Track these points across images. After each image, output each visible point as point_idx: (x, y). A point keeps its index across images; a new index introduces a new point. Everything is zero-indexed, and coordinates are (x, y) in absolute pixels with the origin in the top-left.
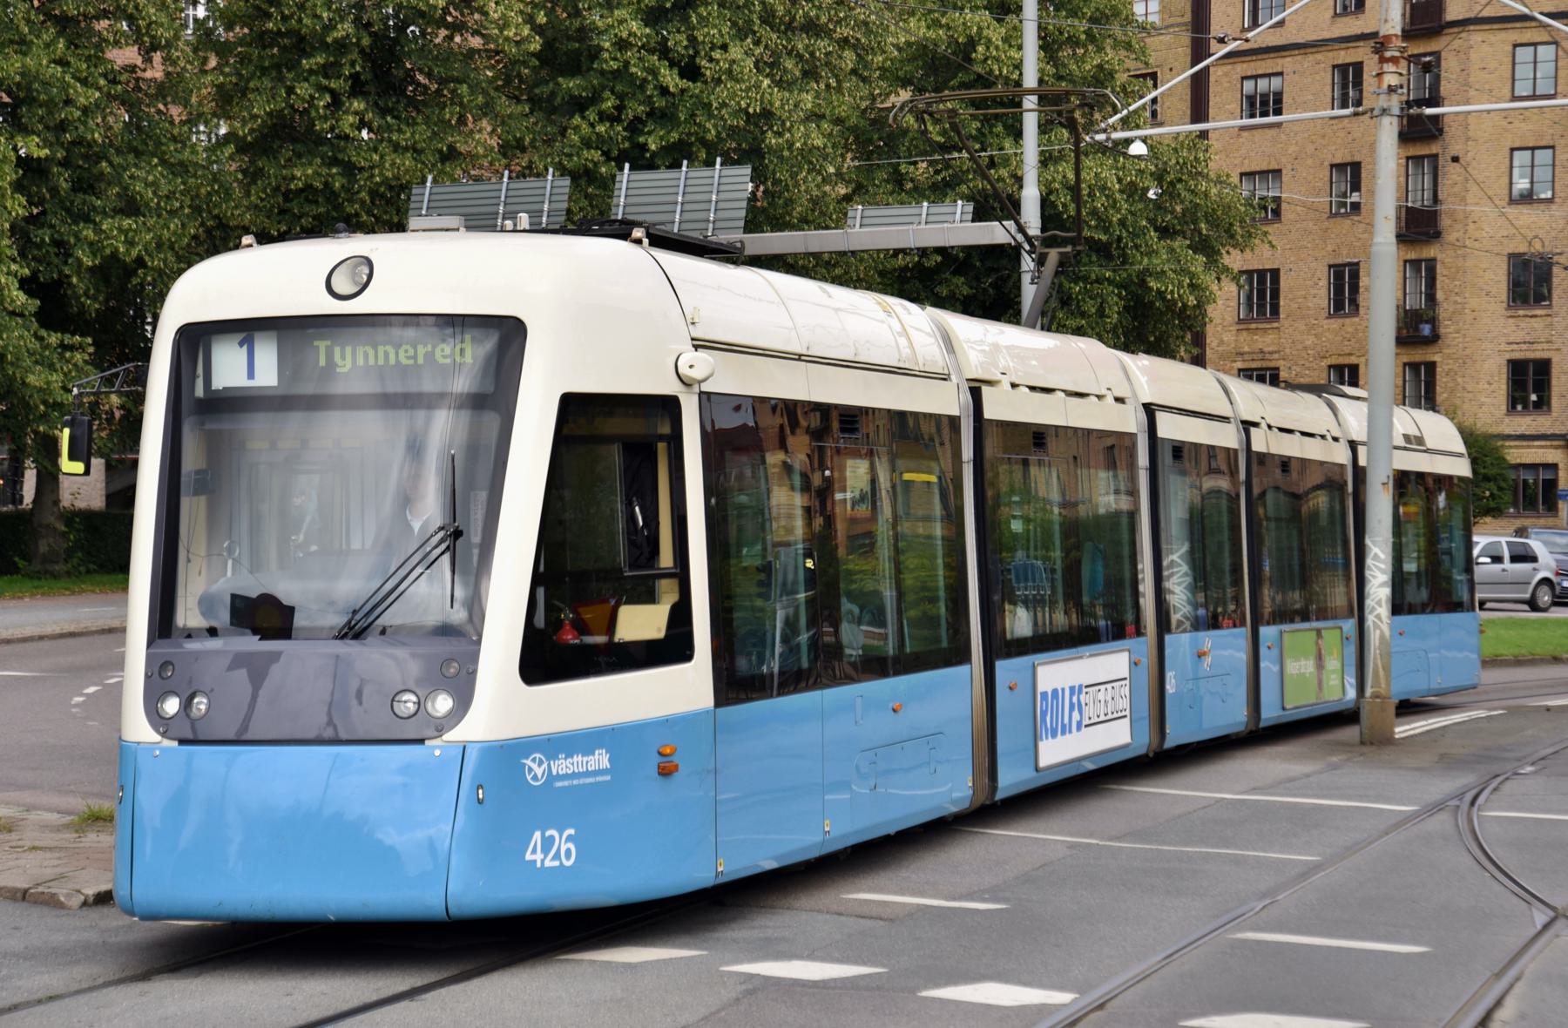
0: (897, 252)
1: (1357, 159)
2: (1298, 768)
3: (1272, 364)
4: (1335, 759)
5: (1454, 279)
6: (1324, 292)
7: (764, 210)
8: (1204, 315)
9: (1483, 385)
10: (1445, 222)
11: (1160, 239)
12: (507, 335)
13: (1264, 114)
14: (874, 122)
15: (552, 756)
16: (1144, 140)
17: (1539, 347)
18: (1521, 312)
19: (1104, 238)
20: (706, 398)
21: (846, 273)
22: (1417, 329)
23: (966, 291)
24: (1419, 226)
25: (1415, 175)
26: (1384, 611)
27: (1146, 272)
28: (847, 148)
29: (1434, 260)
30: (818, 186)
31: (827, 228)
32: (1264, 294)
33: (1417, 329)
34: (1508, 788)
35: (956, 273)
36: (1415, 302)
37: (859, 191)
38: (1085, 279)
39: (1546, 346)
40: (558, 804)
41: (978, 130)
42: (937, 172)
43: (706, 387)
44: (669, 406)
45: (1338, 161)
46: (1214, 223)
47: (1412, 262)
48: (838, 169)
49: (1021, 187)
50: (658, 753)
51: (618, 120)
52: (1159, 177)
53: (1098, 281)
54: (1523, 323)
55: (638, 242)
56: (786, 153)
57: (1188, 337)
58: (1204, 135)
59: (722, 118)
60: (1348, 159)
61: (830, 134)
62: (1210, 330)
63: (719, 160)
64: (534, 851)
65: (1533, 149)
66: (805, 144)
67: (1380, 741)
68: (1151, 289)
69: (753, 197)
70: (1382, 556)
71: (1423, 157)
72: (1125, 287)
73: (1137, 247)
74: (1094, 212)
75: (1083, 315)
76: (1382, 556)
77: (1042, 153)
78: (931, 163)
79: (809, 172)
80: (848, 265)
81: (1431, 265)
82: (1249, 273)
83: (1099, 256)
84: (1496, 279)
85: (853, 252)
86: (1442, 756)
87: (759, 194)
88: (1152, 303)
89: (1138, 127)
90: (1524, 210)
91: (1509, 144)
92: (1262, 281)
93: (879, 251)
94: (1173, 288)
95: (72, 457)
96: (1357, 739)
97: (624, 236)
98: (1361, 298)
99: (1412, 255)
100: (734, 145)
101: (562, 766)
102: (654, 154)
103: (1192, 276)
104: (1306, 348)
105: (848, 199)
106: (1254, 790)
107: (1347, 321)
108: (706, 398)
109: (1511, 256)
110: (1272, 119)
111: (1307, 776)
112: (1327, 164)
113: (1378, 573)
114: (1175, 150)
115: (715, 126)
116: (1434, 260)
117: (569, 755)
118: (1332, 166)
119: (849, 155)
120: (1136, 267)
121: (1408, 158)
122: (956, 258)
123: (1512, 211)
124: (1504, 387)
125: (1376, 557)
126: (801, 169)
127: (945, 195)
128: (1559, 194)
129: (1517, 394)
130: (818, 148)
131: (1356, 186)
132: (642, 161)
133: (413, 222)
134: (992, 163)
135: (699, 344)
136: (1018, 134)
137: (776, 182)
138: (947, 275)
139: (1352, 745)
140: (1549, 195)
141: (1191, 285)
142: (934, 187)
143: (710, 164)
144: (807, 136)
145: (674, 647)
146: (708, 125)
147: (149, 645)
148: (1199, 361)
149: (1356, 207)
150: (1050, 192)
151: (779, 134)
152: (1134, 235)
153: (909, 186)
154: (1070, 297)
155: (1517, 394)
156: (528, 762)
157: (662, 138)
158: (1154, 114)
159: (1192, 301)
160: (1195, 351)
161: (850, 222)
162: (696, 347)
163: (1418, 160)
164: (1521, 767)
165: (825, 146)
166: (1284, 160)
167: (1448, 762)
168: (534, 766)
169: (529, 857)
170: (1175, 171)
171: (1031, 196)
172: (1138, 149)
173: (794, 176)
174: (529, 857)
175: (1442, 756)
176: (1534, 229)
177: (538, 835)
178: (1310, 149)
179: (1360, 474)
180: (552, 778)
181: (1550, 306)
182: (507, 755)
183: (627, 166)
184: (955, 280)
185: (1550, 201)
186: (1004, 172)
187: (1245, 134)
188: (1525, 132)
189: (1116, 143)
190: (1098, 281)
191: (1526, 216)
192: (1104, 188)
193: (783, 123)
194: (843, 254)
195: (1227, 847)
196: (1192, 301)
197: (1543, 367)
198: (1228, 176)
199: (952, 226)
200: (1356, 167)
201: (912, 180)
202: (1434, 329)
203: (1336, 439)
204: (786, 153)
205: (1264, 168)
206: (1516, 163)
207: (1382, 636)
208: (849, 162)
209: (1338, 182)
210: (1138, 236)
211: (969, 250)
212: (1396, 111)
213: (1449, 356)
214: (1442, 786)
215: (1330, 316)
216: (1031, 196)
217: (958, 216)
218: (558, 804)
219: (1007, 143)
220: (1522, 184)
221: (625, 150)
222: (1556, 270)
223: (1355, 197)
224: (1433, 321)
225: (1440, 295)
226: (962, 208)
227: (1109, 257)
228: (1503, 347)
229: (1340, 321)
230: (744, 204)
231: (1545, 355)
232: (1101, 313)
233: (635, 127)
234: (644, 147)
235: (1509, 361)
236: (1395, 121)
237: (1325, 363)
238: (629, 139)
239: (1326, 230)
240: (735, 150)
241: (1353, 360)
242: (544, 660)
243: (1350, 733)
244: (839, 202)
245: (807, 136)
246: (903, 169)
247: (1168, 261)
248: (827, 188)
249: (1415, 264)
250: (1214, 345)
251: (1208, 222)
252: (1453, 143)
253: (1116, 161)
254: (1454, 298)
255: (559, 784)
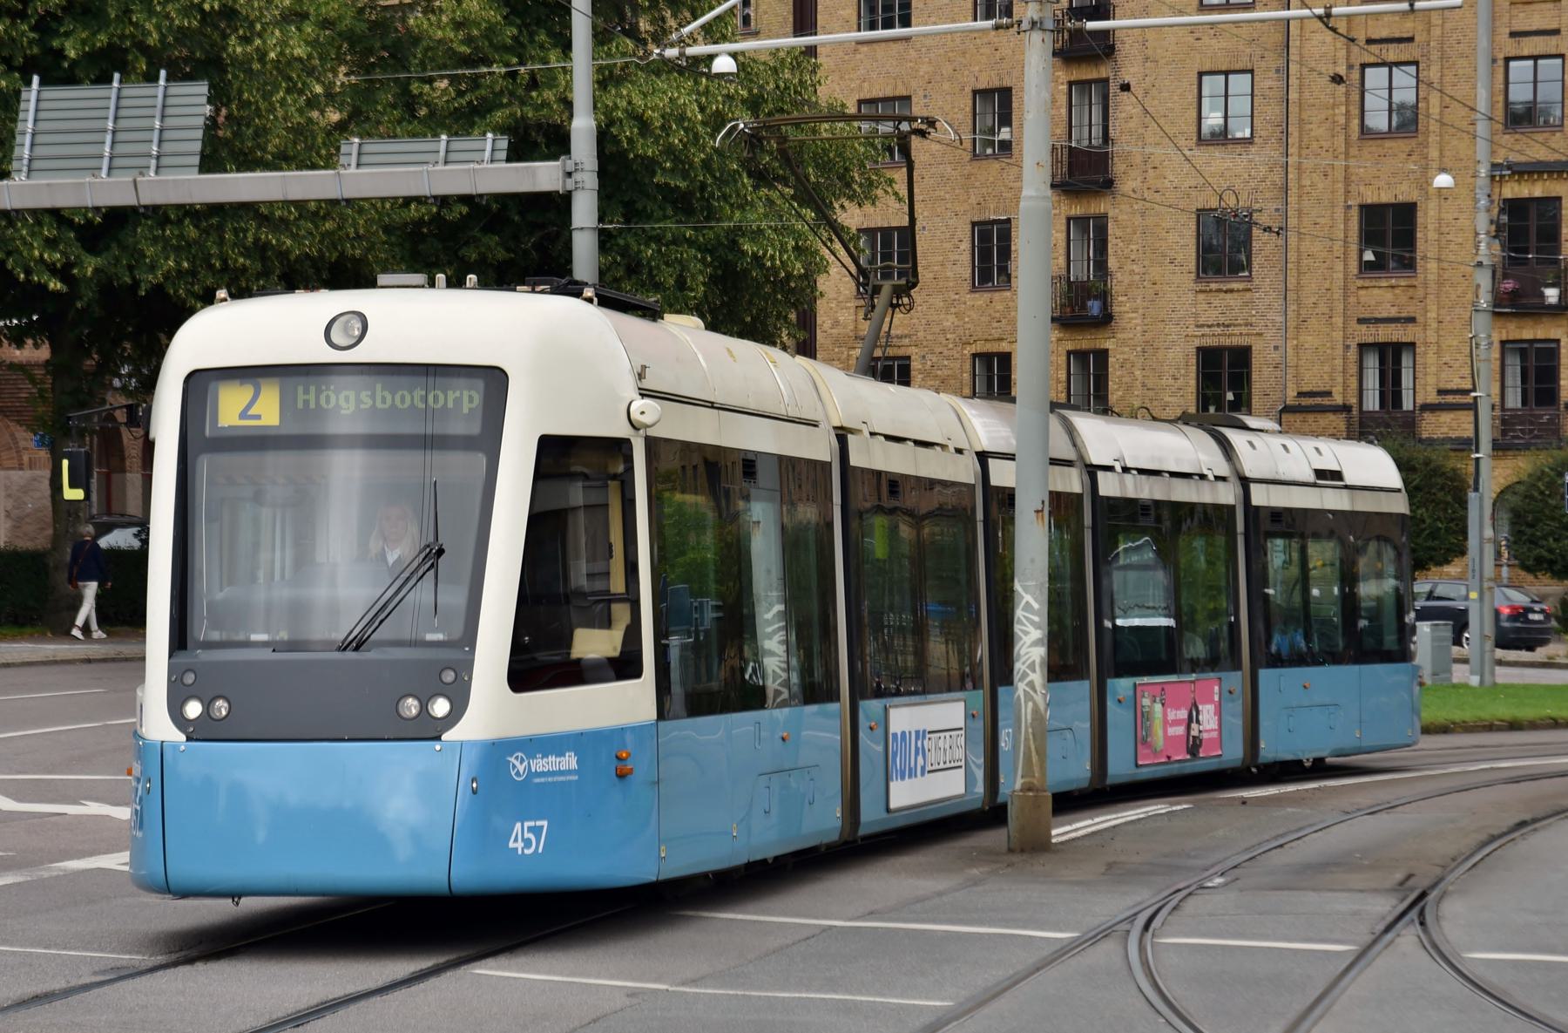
0: (408, 201)
1: (1007, 83)
2: (927, 885)
3: (901, 352)
4: (975, 871)
5: (1130, 242)
6: (966, 257)
7: (226, 142)
8: (814, 288)
9: (1167, 381)
10: (1118, 167)
11: (756, 188)
12: (494, 380)
13: (888, 24)
14: (374, 25)
15: (531, 756)
16: (734, 55)
17: (1236, 330)
18: (1214, 286)
19: (683, 184)
20: (652, 444)
21: (340, 228)
22: (1084, 307)
23: (501, 254)
24: (1084, 172)
25: (1081, 105)
26: (1038, 677)
27: (739, 230)
28: (340, 60)
29: (1105, 217)
30: (300, 111)
31: (314, 167)
32: (891, 264)
33: (1083, 307)
34: (1191, 905)
35: (488, 229)
36: (1082, 271)
37: (359, 120)
38: (658, 239)
39: (1244, 330)
40: (532, 798)
41: (514, 38)
42: (460, 94)
43: (652, 432)
44: (619, 447)
45: (982, 85)
46: (824, 166)
47: (1076, 219)
48: (329, 88)
49: (571, 116)
50: (610, 756)
51: (22, 15)
52: (754, 104)
53: (674, 242)
54: (1217, 300)
55: (590, 300)
56: (256, 66)
57: (793, 316)
58: (811, 51)
59: (167, 16)
60: (996, 84)
61: (316, 40)
62: (821, 305)
63: (163, 73)
64: (516, 840)
65: (1226, 73)
66: (282, 53)
67: (1035, 846)
68: (744, 253)
69: (211, 125)
70: (1036, 606)
71: (1089, 82)
72: (711, 252)
73: (725, 197)
74: (669, 151)
75: (657, 287)
76: (1036, 606)
77: (600, 69)
78: (454, 80)
79: (288, 91)
80: (343, 218)
81: (1101, 223)
82: (870, 232)
83: (676, 209)
84: (1183, 243)
85: (348, 201)
86: (1110, 866)
87: (221, 120)
88: (746, 272)
89: (724, 38)
90: (1217, 152)
91: (1197, 68)
92: (887, 243)
93: (383, 200)
94: (775, 253)
95: (72, 486)
96: (1005, 847)
97: (578, 295)
98: (1012, 266)
99: (1077, 210)
100: (185, 52)
101: (540, 764)
102: (74, 63)
103: (798, 236)
104: (944, 331)
105: (342, 127)
106: (871, 914)
107: (997, 296)
108: (652, 444)
109: (1201, 213)
110: (898, 31)
111: (940, 894)
112: (968, 90)
113: (1031, 628)
114: (775, 71)
115: (158, 27)
116: (1105, 217)
117: (545, 756)
118: (975, 92)
119: (343, 69)
120: (726, 224)
121: (1070, 84)
122: (487, 208)
123: (1201, 156)
124: (1193, 382)
125: (1028, 607)
126: (277, 88)
127: (472, 125)
128: (1260, 132)
129: (1209, 392)
130: (300, 59)
131: (1006, 120)
132: (58, 73)
133: (382, 279)
134: (534, 83)
135: (645, 393)
136: (566, 46)
137: (244, 105)
138: (476, 233)
139: (998, 854)
140: (1247, 134)
141: (797, 248)
142: (457, 114)
143: (151, 78)
144: (283, 43)
145: (624, 666)
146: (148, 26)
147: (170, 656)
148: (807, 349)
149: (1006, 146)
150: (611, 122)
151: (246, 40)
152: (721, 182)
153: (423, 112)
154: (639, 264)
155: (1209, 392)
156: (512, 760)
157: (84, 42)
158: (746, 20)
159: (799, 268)
160: (801, 335)
161: (343, 160)
162: (643, 396)
163: (1084, 85)
164: (1209, 878)
165: (310, 56)
166: (914, 84)
167: (1117, 873)
168: (517, 763)
169: (511, 845)
170: (776, 98)
171: (583, 126)
172: (724, 64)
173: (267, 96)
174: (511, 845)
175: (1110, 866)
176: (1235, 178)
177: (518, 825)
178: (947, 69)
179: (1004, 500)
180: (531, 775)
181: (1250, 278)
182: (497, 751)
183: (36, 79)
184: (485, 240)
185: (1249, 141)
186: (549, 95)
187: (864, 49)
188: (1216, 51)
189: (696, 60)
190: (674, 242)
191: (1217, 161)
192: (682, 118)
193: (252, 25)
194: (334, 203)
195: (835, 992)
196: (799, 268)
197: (1241, 357)
198: (843, 105)
199: (480, 168)
200: (1005, 94)
201: (427, 104)
202: (1105, 306)
203: (959, 451)
204: (256, 66)
205: (889, 93)
206: (1205, 92)
207: (1036, 711)
208: (342, 78)
209: (983, 114)
210: (727, 183)
211: (505, 199)
212: (1050, 25)
213: (1124, 343)
214: (1111, 905)
215: (974, 289)
216: (583, 126)
217: (487, 154)
218: (532, 798)
219: (553, 56)
220: (1213, 119)
221: (33, 57)
222: (1256, 232)
223: (1005, 133)
224: (1105, 297)
225: (1112, 263)
226: (491, 143)
227: (689, 211)
228: (1192, 330)
229: (987, 296)
230: (199, 134)
231: (1243, 341)
232: (681, 284)
233: (46, 25)
234: (60, 54)
235: (1199, 349)
236: (1049, 37)
237: (969, 350)
238: (39, 42)
239: (968, 177)
240: (186, 60)
241: (1004, 347)
242: (535, 666)
243: (993, 838)
244: (329, 134)
245: (283, 43)
246: (415, 88)
247: (766, 216)
248: (315, 114)
249: (1080, 222)
250: (827, 325)
251: (817, 166)
252: (1129, 67)
253: (696, 82)
254: (1129, 266)
255: (537, 780)
